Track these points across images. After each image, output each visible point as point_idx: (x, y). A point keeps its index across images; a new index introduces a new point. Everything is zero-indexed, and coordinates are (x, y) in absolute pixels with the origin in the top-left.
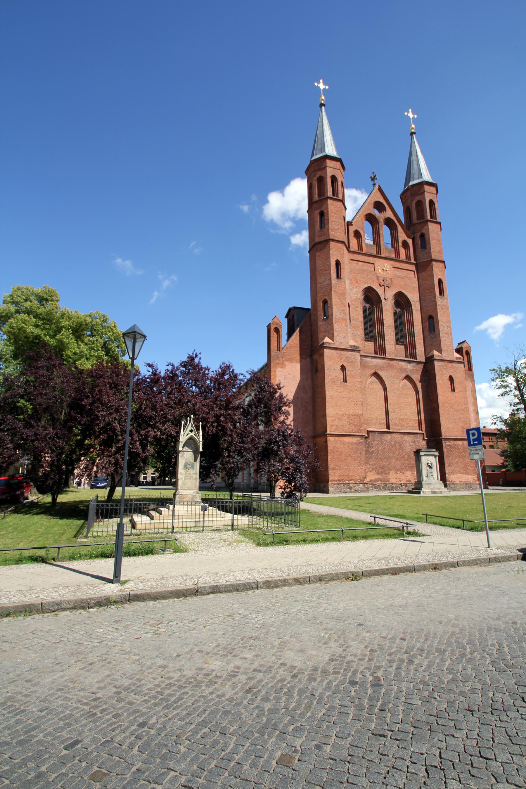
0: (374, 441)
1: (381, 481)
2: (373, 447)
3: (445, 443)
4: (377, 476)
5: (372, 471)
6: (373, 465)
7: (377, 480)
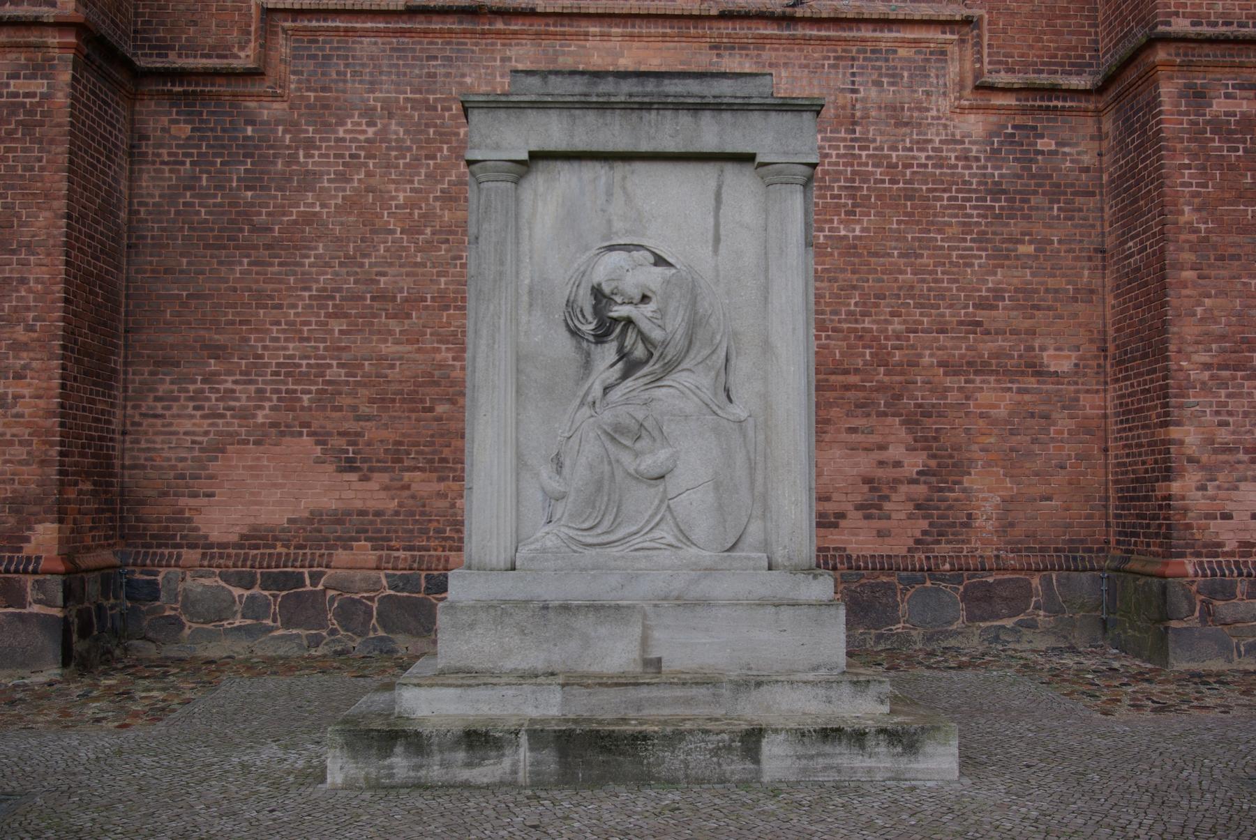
0: (325, 112)
1: (379, 542)
2: (309, 180)
3: (1198, 96)
4: (328, 492)
5: (281, 430)
6: (288, 369)
7: (326, 531)
